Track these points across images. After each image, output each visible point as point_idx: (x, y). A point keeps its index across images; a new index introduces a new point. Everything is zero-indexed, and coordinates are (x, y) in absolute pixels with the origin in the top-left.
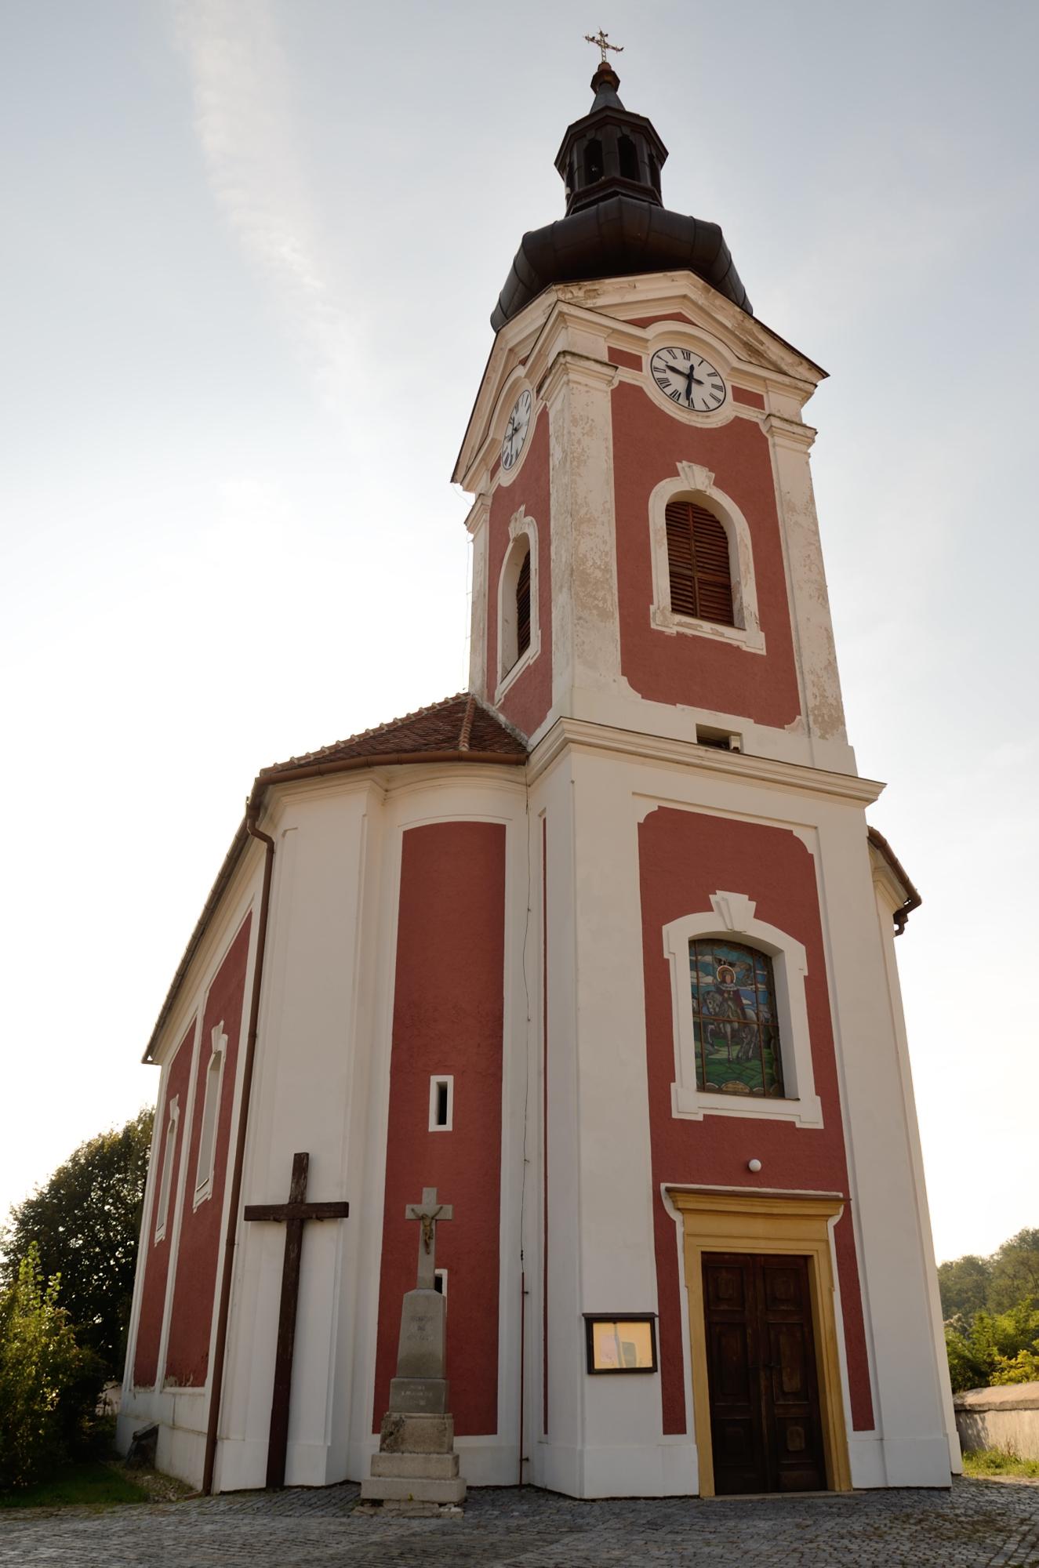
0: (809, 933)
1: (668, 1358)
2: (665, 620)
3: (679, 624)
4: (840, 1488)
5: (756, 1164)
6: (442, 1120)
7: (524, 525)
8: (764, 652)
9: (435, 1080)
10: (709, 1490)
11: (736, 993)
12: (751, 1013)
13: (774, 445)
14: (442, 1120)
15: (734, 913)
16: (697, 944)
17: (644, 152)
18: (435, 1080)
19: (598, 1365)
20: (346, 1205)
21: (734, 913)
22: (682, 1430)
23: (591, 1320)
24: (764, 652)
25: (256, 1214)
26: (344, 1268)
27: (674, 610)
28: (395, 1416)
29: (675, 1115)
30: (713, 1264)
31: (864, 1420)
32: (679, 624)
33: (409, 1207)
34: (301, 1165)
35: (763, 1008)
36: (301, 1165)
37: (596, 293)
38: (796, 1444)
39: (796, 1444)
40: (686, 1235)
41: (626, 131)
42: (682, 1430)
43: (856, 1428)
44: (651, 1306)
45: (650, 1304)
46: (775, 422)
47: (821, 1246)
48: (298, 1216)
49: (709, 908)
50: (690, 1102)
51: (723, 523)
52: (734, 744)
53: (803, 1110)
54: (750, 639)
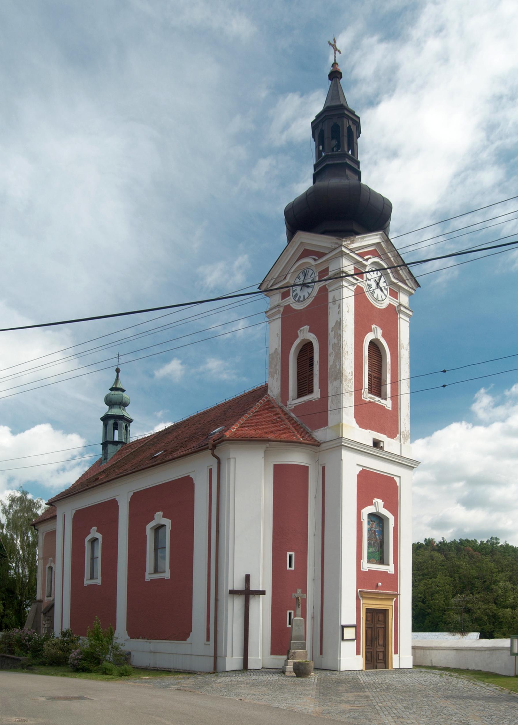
0: (395, 511)
1: (358, 637)
2: (367, 396)
3: (370, 398)
4: (390, 668)
5: (380, 584)
6: (290, 566)
7: (305, 334)
8: (391, 409)
9: (289, 553)
10: (364, 669)
11: (375, 531)
12: (378, 537)
13: (400, 318)
14: (290, 566)
15: (378, 506)
16: (370, 515)
17: (347, 123)
18: (289, 553)
19: (345, 638)
20: (265, 591)
21: (378, 506)
22: (360, 654)
23: (343, 627)
24: (391, 409)
25: (233, 592)
26: (261, 610)
27: (369, 393)
28: (293, 651)
29: (362, 570)
30: (368, 611)
31: (396, 652)
32: (370, 398)
33: (293, 594)
34: (248, 578)
35: (381, 536)
36: (248, 578)
37: (352, 242)
38: (381, 657)
39: (381, 657)
40: (363, 604)
41: (351, 123)
42: (360, 654)
43: (395, 654)
44: (354, 623)
45: (354, 623)
46: (402, 308)
47: (391, 607)
48: (247, 594)
49: (372, 504)
50: (366, 566)
51: (381, 351)
52: (381, 445)
53: (390, 569)
54: (388, 404)
